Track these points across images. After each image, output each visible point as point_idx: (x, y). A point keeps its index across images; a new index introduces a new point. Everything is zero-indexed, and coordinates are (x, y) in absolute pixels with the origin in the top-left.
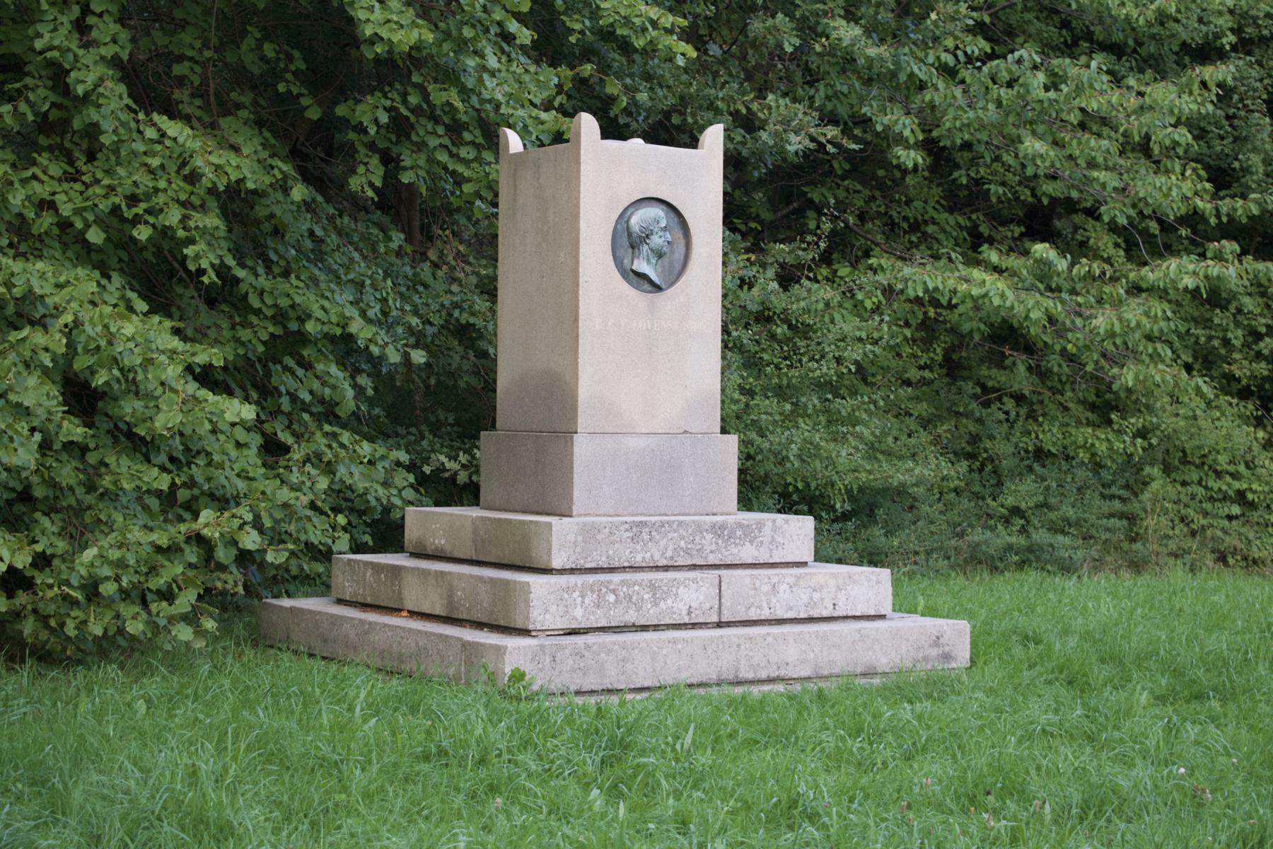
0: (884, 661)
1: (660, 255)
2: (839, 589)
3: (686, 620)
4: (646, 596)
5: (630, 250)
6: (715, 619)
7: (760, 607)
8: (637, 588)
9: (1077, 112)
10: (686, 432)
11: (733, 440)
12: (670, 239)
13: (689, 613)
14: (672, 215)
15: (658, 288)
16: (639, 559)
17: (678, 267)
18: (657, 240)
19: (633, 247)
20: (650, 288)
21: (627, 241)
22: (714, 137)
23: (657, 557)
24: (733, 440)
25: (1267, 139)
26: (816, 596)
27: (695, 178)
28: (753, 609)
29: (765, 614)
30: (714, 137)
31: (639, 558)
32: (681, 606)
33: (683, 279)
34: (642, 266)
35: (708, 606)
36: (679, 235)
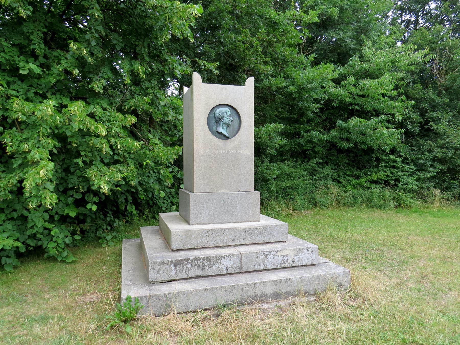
0: (311, 289)
1: (228, 126)
2: (295, 255)
3: (225, 272)
4: (206, 264)
5: (216, 124)
6: (238, 271)
7: (260, 265)
8: (201, 261)
9: (297, 209)
10: (240, 191)
11: (258, 193)
12: (232, 119)
13: (227, 269)
14: (233, 110)
15: (228, 138)
16: (212, 244)
17: (236, 130)
18: (226, 120)
19: (217, 123)
20: (224, 138)
21: (214, 120)
22: (250, 81)
23: (219, 242)
24: (258, 193)
25: (60, 132)
26: (285, 259)
27: (243, 96)
28: (256, 266)
29: (262, 267)
30: (250, 81)
31: (211, 243)
32: (223, 267)
33: (238, 134)
34: (221, 130)
35: (235, 266)
36: (236, 118)
